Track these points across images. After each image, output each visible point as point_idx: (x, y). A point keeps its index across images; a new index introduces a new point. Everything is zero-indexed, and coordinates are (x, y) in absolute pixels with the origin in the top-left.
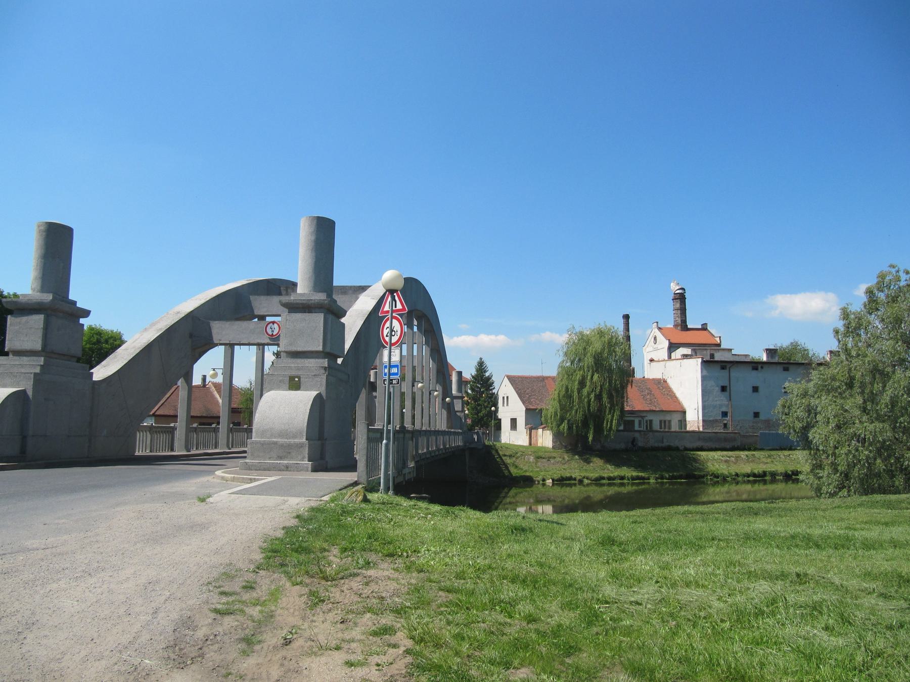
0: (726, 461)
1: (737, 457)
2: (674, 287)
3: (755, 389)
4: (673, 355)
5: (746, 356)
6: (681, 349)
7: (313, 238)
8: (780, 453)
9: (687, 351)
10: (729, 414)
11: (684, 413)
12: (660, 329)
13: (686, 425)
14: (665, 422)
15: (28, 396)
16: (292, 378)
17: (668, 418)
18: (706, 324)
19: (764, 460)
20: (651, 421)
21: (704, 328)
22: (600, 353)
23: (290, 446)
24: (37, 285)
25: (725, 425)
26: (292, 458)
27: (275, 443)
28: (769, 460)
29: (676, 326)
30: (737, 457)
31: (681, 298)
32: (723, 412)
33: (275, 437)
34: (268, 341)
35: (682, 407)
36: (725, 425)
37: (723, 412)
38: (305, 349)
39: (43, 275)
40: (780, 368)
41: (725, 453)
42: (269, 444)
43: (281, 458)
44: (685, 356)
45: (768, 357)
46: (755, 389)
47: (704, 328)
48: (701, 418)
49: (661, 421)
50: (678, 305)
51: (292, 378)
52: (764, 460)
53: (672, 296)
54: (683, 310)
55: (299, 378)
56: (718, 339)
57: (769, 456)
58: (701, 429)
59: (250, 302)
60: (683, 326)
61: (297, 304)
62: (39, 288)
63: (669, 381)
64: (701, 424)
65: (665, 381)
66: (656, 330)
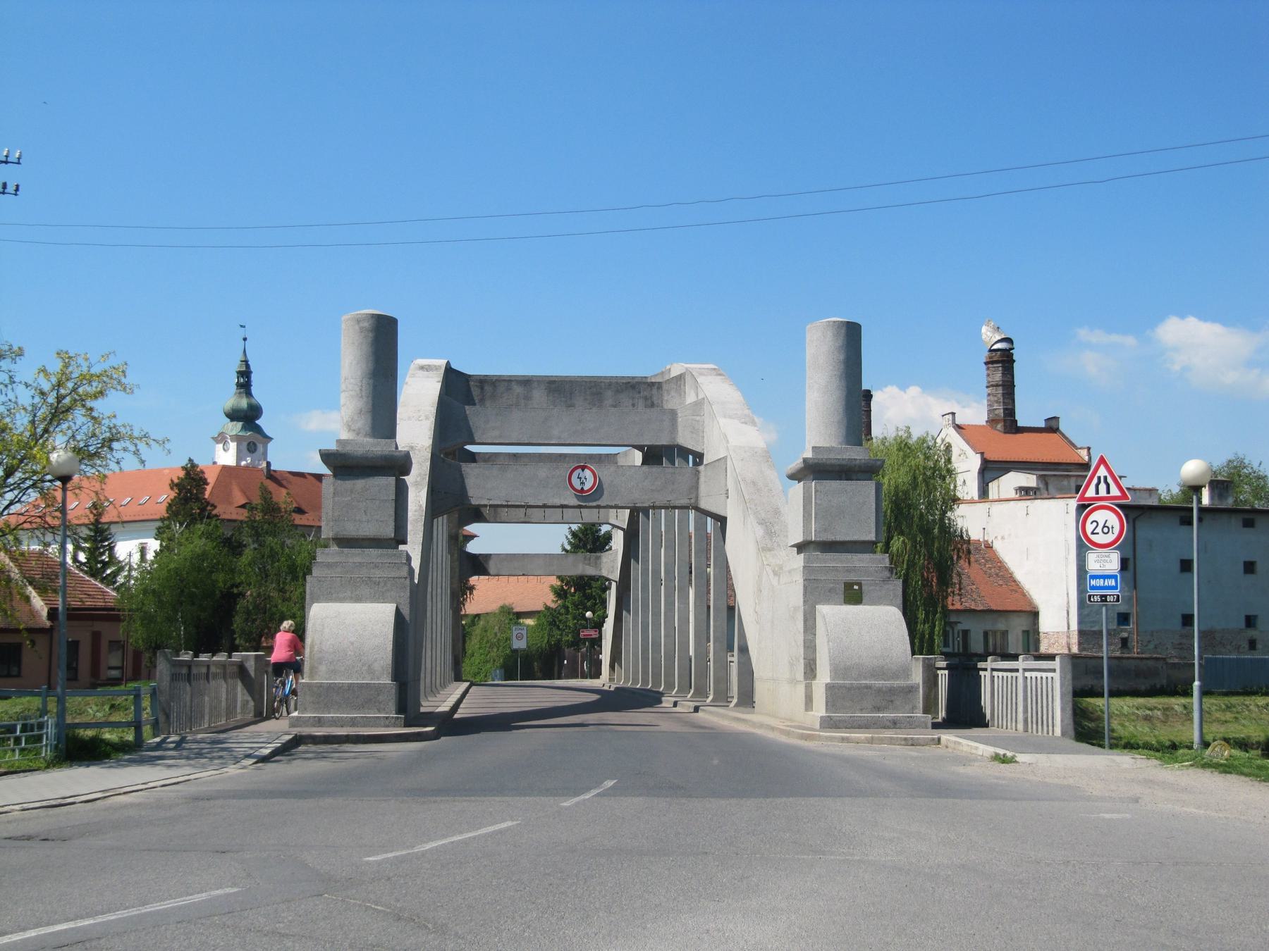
0: (1147, 718)
1: (1167, 709)
2: (989, 337)
3: (1249, 567)
4: (993, 487)
5: (1152, 491)
6: (1012, 475)
7: (842, 357)
8: (1248, 700)
9: (1029, 480)
10: (1133, 620)
11: (1035, 615)
12: (959, 428)
13: (1037, 642)
14: (995, 632)
15: (404, 618)
16: (848, 586)
17: (1001, 626)
18: (1056, 419)
19: (1218, 715)
20: (966, 633)
21: (1052, 427)
22: (906, 493)
23: (892, 691)
24: (363, 423)
25: (1125, 642)
26: (896, 710)
27: (868, 687)
28: (1229, 716)
29: (992, 421)
30: (1167, 709)
31: (1003, 360)
32: (1119, 615)
33: (865, 678)
34: (574, 502)
35: (1029, 601)
36: (1125, 642)
37: (1119, 615)
38: (848, 539)
39: (373, 405)
40: (1236, 522)
41: (1141, 701)
42: (859, 688)
43: (878, 709)
44: (1026, 493)
45: (1212, 498)
46: (1249, 567)
47: (1052, 427)
48: (1074, 626)
49: (986, 634)
50: (998, 376)
51: (848, 586)
52: (1218, 715)
53: (984, 356)
54: (1007, 388)
55: (860, 584)
56: (1084, 453)
57: (1229, 708)
58: (1075, 650)
59: (466, 418)
60: (1007, 421)
61: (832, 465)
62: (368, 428)
63: (997, 546)
64: (1075, 639)
65: (989, 547)
66: (952, 431)
